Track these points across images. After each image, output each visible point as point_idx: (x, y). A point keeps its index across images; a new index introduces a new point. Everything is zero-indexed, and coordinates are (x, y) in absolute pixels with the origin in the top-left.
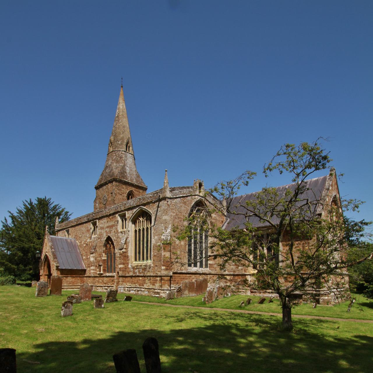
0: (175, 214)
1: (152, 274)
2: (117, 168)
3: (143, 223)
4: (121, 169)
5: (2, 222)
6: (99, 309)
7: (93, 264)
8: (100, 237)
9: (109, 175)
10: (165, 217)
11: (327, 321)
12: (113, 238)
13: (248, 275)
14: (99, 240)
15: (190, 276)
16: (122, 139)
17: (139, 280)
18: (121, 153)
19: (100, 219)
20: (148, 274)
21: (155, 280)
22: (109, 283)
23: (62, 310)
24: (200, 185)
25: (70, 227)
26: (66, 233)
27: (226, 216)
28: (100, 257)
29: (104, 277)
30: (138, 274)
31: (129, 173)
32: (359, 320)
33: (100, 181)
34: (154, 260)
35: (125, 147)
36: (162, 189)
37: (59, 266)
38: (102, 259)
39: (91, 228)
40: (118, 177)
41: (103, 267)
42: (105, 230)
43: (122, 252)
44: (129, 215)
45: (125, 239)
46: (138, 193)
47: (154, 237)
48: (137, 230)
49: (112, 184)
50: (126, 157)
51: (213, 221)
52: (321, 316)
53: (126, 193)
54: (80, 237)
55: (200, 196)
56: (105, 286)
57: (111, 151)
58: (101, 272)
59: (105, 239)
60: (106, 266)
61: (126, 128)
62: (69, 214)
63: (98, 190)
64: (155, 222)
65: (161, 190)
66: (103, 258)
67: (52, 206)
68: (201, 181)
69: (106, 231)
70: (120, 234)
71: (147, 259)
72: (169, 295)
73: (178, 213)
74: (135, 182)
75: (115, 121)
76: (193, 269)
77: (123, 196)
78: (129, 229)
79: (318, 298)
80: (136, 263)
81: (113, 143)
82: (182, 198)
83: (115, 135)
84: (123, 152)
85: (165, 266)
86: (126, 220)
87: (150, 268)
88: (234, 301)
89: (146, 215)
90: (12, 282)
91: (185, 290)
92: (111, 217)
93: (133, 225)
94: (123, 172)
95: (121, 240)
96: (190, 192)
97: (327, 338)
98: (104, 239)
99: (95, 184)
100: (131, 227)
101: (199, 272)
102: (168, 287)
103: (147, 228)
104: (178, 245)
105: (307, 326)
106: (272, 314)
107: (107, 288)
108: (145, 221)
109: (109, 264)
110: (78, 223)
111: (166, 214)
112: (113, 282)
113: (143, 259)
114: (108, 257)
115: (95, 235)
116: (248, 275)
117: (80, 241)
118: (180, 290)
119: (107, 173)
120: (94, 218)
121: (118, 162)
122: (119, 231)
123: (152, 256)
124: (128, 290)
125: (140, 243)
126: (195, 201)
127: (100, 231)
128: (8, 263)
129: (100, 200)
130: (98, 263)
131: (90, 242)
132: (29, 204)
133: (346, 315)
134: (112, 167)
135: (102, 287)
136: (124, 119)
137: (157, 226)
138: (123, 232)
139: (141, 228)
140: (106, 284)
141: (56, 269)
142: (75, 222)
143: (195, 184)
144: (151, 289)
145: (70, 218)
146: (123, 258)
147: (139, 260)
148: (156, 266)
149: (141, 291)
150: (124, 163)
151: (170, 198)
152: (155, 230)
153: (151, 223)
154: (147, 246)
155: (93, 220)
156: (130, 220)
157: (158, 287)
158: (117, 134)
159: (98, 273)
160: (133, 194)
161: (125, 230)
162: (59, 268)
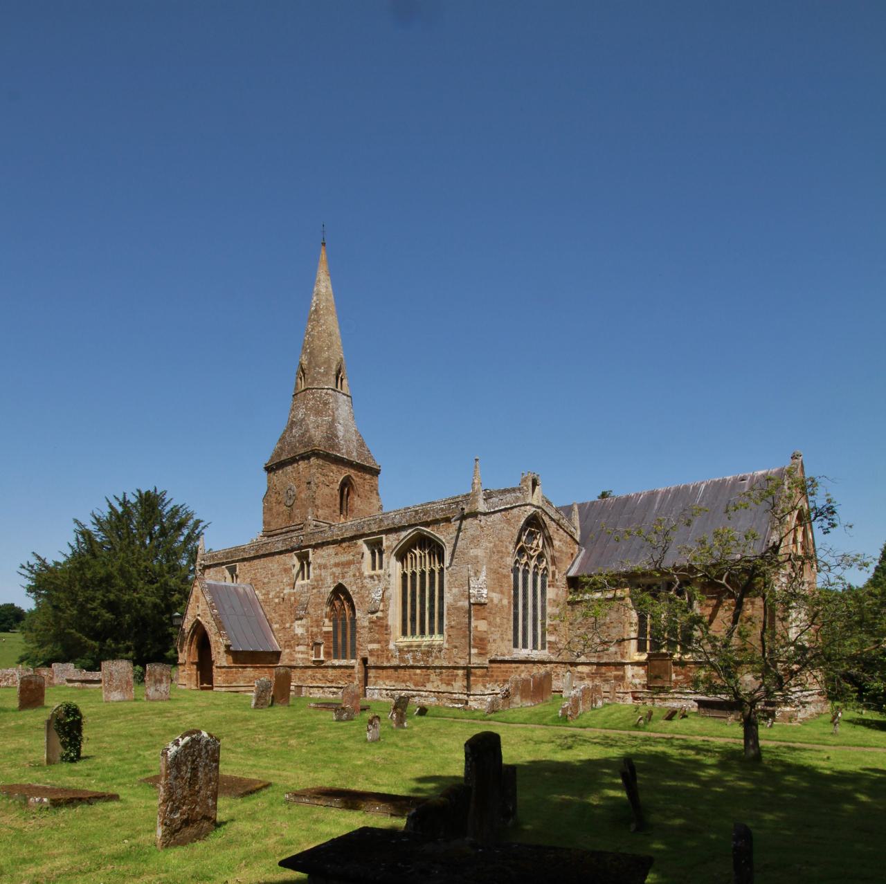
0: (492, 545)
1: (445, 664)
2: (318, 426)
3: (421, 561)
4: (327, 429)
5: (70, 546)
6: (401, 730)
7: (301, 642)
8: (318, 585)
9: (300, 442)
10: (473, 552)
11: (804, 750)
12: (351, 589)
13: (628, 664)
14: (315, 591)
15: (517, 668)
16: (328, 361)
17: (415, 674)
18: (326, 394)
19: (316, 547)
20: (437, 663)
21: (452, 676)
22: (341, 680)
23: (369, 730)
24: (535, 483)
25: (238, 561)
26: (227, 573)
27: (578, 543)
28: (318, 626)
29: (327, 667)
30: (411, 663)
31: (343, 436)
32: (856, 748)
33: (278, 453)
34: (450, 636)
35: (333, 379)
36: (468, 495)
37: (231, 646)
38: (321, 630)
39: (294, 566)
40: (322, 448)
41: (325, 647)
42: (330, 571)
43: (377, 617)
44: (389, 543)
45: (381, 592)
46: (362, 481)
47: (450, 590)
48: (409, 573)
49: (309, 462)
50: (336, 401)
51: (557, 554)
52: (790, 742)
53: (338, 481)
54: (264, 584)
55: (533, 506)
56: (332, 687)
57: (303, 388)
58: (319, 657)
59: (331, 589)
60: (332, 645)
61: (334, 338)
62: (202, 525)
63: (272, 474)
64: (452, 560)
65: (465, 496)
66: (325, 629)
67: (168, 508)
68: (536, 476)
69: (333, 574)
70: (368, 580)
71: (432, 632)
72: (492, 703)
73: (497, 542)
74: (356, 458)
75: (309, 320)
76: (522, 653)
77: (333, 489)
78: (391, 571)
79: (771, 709)
80: (405, 639)
81: (306, 371)
82: (503, 513)
83: (310, 353)
84: (330, 391)
85: (477, 648)
86: (381, 553)
87: (440, 651)
88: (615, 715)
89: (429, 546)
90: (140, 678)
91: (515, 695)
92: (344, 545)
93: (399, 564)
94: (331, 437)
95: (369, 593)
96: (517, 499)
97: (820, 771)
98: (329, 586)
99: (266, 459)
100: (394, 568)
101: (532, 658)
102: (482, 688)
103: (432, 572)
104: (497, 605)
105: (778, 756)
106: (706, 738)
107: (335, 690)
108: (427, 557)
109: (340, 641)
110: (261, 552)
111: (477, 546)
112: (350, 679)
113: (423, 632)
114: (335, 627)
115: (303, 579)
116: (628, 664)
117: (264, 592)
118: (507, 696)
119: (294, 437)
120: (302, 544)
121: (318, 413)
122: (366, 574)
123: (445, 628)
124: (387, 695)
125: (413, 600)
126: (526, 516)
127: (317, 572)
128: (81, 635)
129: (277, 495)
130: (312, 638)
131: (290, 595)
132: (120, 504)
133: (832, 740)
134: (308, 425)
135: (322, 688)
136: (331, 318)
137: (457, 568)
138: (375, 577)
139: (418, 571)
140: (332, 682)
141: (226, 652)
142: (253, 550)
143: (525, 481)
144: (443, 693)
145: (203, 534)
146: (378, 630)
147: (413, 633)
148: (456, 647)
149: (421, 696)
150: (333, 416)
151: (485, 514)
152: (451, 575)
153: (441, 560)
154: (432, 606)
155: (300, 548)
156: (392, 553)
157: (459, 690)
158: (315, 352)
159: (314, 659)
160: (352, 484)
161: (378, 572)
162: (232, 648)
